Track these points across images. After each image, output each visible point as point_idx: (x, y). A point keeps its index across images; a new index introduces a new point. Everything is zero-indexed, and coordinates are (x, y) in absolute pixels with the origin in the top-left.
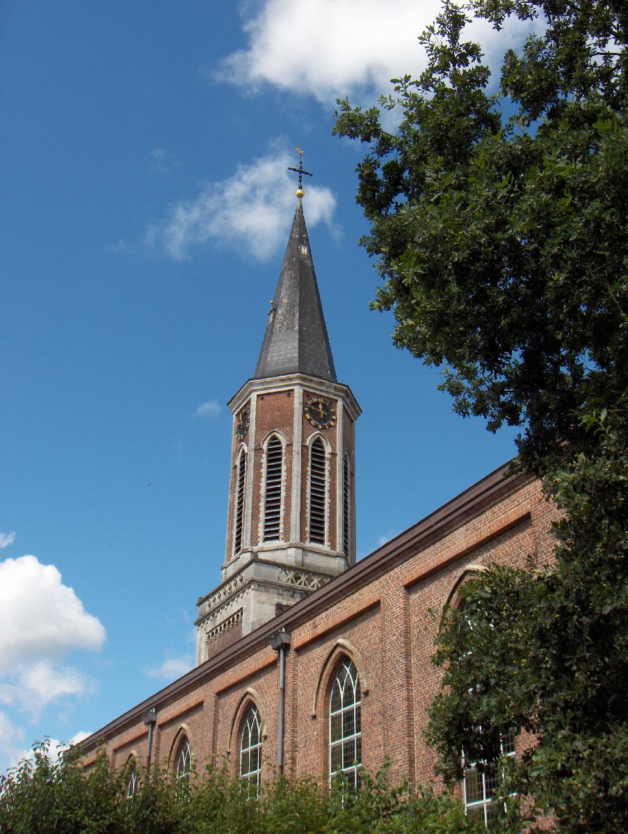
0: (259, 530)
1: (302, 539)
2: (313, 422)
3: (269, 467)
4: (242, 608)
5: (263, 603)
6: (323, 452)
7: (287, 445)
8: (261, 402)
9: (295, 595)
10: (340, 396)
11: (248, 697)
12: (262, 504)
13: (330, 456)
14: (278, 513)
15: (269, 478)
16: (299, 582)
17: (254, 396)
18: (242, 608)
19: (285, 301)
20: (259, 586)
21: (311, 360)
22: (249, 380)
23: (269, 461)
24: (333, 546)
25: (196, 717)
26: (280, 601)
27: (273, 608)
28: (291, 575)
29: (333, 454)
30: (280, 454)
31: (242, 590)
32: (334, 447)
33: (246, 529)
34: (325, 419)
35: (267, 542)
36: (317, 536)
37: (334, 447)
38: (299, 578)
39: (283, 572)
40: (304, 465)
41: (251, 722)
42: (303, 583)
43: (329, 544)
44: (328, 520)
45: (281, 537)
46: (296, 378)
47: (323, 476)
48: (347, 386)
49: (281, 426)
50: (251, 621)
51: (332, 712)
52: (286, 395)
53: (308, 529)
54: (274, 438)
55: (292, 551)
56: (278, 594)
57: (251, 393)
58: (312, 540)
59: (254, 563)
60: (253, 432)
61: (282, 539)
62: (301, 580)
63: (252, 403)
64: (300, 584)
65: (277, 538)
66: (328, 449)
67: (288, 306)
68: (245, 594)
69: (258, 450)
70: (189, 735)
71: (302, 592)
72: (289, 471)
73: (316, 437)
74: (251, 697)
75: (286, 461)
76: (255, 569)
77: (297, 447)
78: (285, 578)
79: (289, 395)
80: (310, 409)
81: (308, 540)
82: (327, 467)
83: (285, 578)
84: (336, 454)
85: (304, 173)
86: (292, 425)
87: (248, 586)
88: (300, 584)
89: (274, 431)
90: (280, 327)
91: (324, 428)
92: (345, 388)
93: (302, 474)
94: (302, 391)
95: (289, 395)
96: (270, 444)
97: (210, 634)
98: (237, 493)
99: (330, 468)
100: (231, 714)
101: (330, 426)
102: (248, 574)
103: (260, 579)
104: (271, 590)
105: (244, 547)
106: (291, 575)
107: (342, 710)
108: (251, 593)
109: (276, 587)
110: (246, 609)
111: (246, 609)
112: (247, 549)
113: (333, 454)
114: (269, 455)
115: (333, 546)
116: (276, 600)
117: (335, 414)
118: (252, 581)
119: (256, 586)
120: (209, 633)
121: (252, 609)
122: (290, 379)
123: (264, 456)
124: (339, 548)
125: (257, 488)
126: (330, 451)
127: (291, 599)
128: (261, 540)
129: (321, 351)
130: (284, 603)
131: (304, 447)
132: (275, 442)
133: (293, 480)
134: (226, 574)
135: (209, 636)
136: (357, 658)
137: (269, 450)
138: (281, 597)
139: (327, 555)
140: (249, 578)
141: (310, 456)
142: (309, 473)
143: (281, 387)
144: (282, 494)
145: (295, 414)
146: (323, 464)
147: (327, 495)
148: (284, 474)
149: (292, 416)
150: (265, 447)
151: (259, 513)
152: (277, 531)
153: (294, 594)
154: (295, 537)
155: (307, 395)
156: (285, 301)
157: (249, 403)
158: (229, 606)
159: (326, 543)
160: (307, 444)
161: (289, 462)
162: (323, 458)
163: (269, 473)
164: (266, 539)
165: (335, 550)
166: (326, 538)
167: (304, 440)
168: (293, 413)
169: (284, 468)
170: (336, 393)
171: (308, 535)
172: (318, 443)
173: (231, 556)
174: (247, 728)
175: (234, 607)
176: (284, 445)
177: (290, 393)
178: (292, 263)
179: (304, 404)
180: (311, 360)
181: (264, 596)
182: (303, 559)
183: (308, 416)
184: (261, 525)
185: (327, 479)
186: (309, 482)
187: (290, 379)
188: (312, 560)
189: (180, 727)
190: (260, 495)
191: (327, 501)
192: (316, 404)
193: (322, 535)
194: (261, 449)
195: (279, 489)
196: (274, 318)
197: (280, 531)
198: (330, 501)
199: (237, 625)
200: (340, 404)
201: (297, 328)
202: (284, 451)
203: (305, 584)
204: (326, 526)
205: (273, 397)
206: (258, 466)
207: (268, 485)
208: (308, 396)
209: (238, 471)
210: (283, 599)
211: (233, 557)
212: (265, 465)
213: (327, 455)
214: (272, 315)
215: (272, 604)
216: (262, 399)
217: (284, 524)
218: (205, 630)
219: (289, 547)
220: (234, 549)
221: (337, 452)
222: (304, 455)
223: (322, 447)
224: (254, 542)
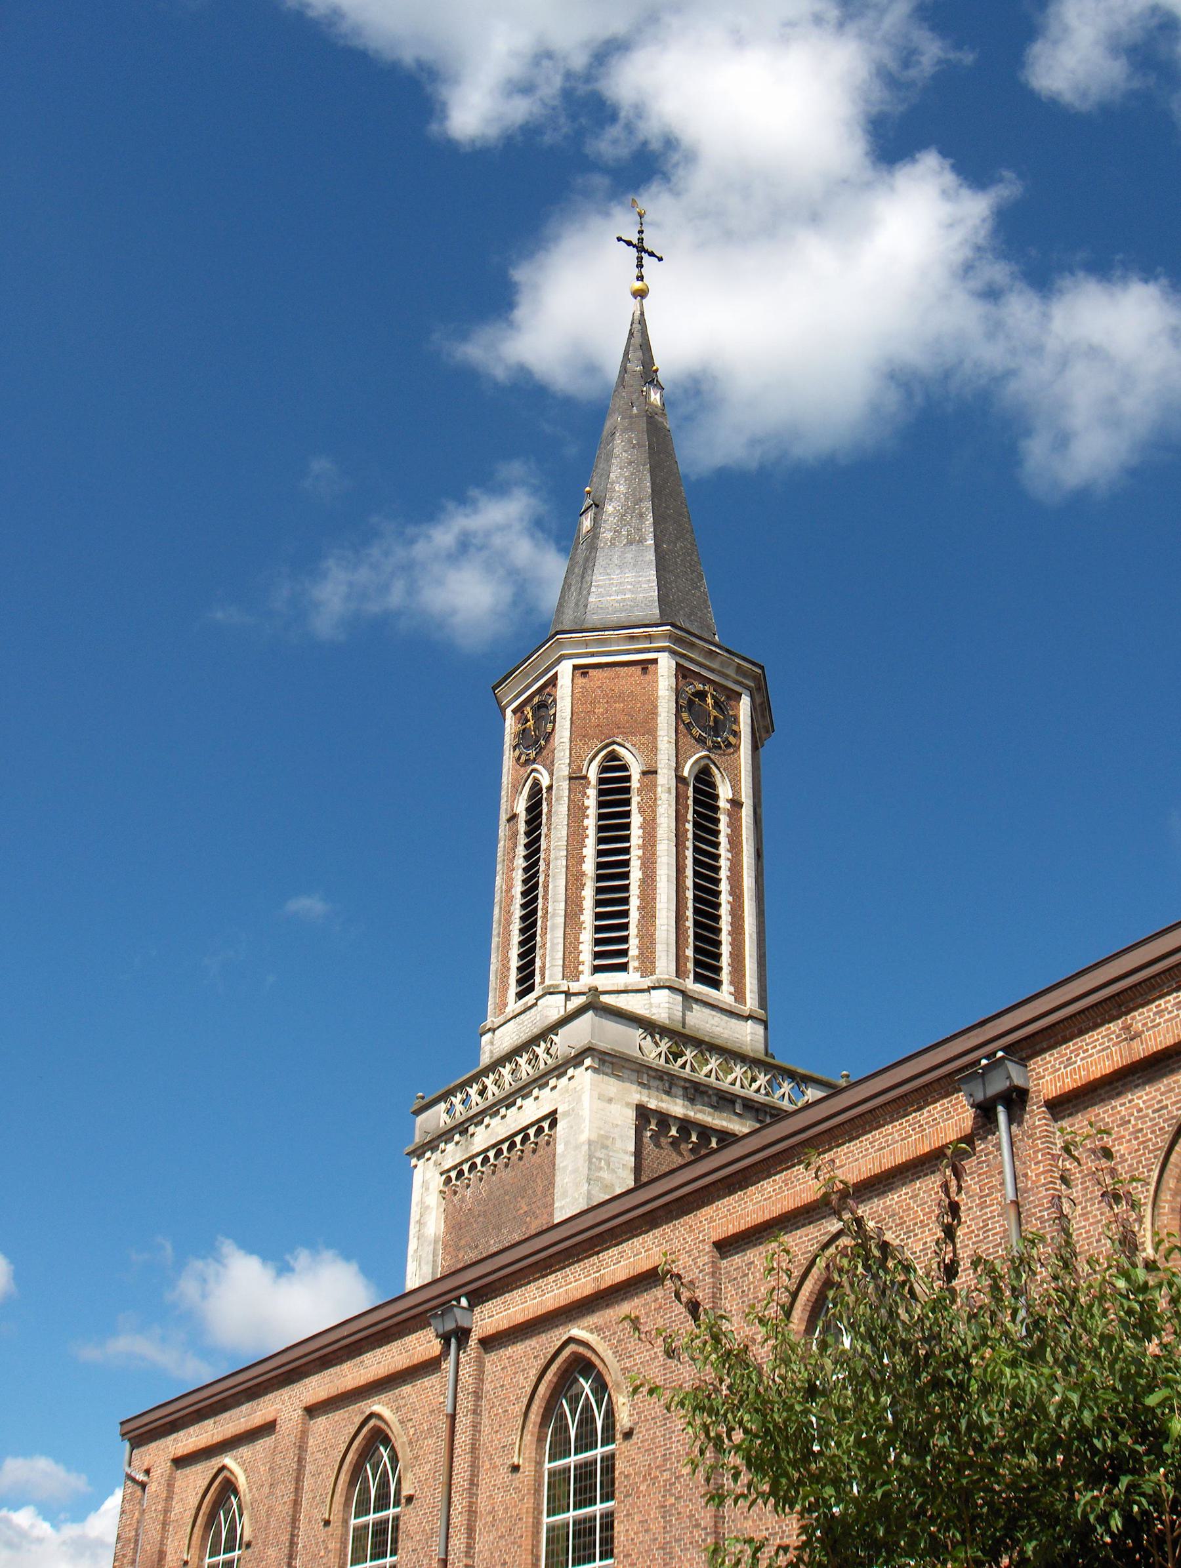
0: (581, 947)
1: (680, 972)
2: (696, 731)
3: (601, 817)
4: (555, 1112)
5: (610, 1100)
6: (716, 797)
7: (644, 773)
8: (581, 681)
9: (674, 1090)
10: (747, 687)
11: (225, 1473)
12: (588, 894)
13: (728, 806)
14: (625, 914)
15: (600, 841)
16: (680, 1061)
17: (565, 670)
18: (555, 1112)
19: (621, 488)
20: (602, 1062)
21: (682, 608)
22: (557, 633)
23: (601, 805)
24: (739, 995)
25: (263, 1445)
26: (645, 1099)
27: (631, 1114)
28: (665, 1045)
29: (736, 803)
30: (627, 790)
31: (559, 1070)
32: (736, 787)
33: (553, 945)
34: (717, 729)
35: (598, 975)
36: (708, 972)
37: (736, 787)
38: (681, 1055)
39: (649, 1038)
40: (679, 819)
41: (375, 1468)
42: (688, 1066)
43: (732, 989)
44: (729, 938)
45: (633, 964)
46: (663, 636)
47: (716, 845)
48: (762, 668)
49: (629, 732)
50: (584, 1137)
51: (550, 1462)
52: (637, 670)
53: (690, 952)
54: (613, 756)
55: (662, 997)
56: (640, 1084)
57: (558, 661)
58: (699, 978)
59: (590, 1014)
60: (567, 740)
61: (637, 970)
62: (684, 1059)
63: (560, 682)
64: (683, 1066)
65: (623, 967)
66: (724, 792)
67: (627, 499)
68: (564, 1080)
69: (577, 779)
70: (242, 1481)
71: (687, 1085)
72: (650, 826)
73: (703, 763)
74: (229, 1474)
75: (640, 808)
76: (593, 1025)
77: (665, 778)
78: (653, 1051)
79: (645, 670)
80: (690, 700)
81: (691, 976)
82: (723, 826)
83: (653, 1051)
84: (742, 805)
85: (646, 251)
86: (652, 732)
87: (576, 1060)
88: (683, 1066)
89: (614, 743)
90: (613, 539)
91: (717, 746)
92: (759, 671)
93: (677, 836)
94: (673, 663)
95: (645, 670)
96: (604, 769)
97: (453, 1174)
98: (520, 872)
99: (729, 831)
100: (194, 1501)
101: (729, 745)
102: (567, 1041)
103: (603, 1046)
104: (626, 1073)
105: (548, 982)
106: (665, 1045)
107: (572, 1460)
108: (583, 1077)
109: (634, 1067)
110: (567, 1114)
111: (567, 1114)
112: (557, 986)
113: (736, 803)
114: (601, 793)
115: (739, 995)
116: (637, 1095)
117: (736, 720)
118: (588, 1051)
119: (597, 1060)
120: (449, 1171)
121: (586, 1112)
122: (650, 638)
123: (592, 792)
124: (751, 1002)
125: (575, 857)
126: (730, 796)
127: (664, 1097)
128: (586, 968)
129: (698, 594)
130: (652, 1104)
131: (680, 779)
132: (614, 767)
133: (659, 847)
134: (492, 1043)
135: (449, 1179)
136: (399, 1437)
137: (601, 781)
138: (645, 1091)
139: (731, 1014)
140: (581, 1043)
141: (690, 802)
142: (690, 835)
143: (628, 652)
144: (632, 875)
145: (660, 709)
146: (716, 821)
147: (724, 887)
148: (636, 833)
149: (654, 713)
150: (593, 774)
151: (581, 911)
152: (624, 953)
153: (670, 1088)
154: (665, 966)
155: (682, 673)
156: (621, 488)
157: (553, 681)
158: (514, 1109)
159: (726, 987)
160: (686, 774)
161: (650, 808)
162: (716, 809)
163: (600, 829)
164: (597, 969)
165: (744, 1002)
166: (725, 976)
167: (678, 767)
168: (656, 707)
169: (636, 820)
170: (741, 679)
171: (690, 965)
172: (704, 780)
173: (506, 1005)
174: (366, 1479)
175: (530, 1110)
176: (635, 772)
177: (646, 666)
178: (631, 417)
179: (678, 692)
180: (682, 608)
181: (612, 1086)
182: (684, 1015)
183: (685, 715)
184: (587, 937)
185: (724, 850)
186: (689, 853)
187: (650, 638)
188: (702, 1021)
189: (220, 1465)
190: (583, 874)
191: (725, 898)
192: (702, 695)
193: (718, 970)
194: (585, 777)
195: (626, 863)
196: (596, 521)
197: (631, 953)
198: (731, 899)
199: (534, 1151)
200: (745, 703)
201: (651, 542)
202: (635, 784)
203: (693, 1070)
204: (725, 950)
205: (608, 672)
206: (576, 812)
207: (600, 853)
208: (684, 677)
209: (522, 827)
210: (649, 1096)
211: (513, 1006)
212: (592, 812)
213: (722, 804)
214: (590, 514)
215: (628, 1104)
216: (585, 674)
217: (641, 937)
218: (437, 1164)
219: (654, 988)
220: (513, 989)
221: (743, 800)
222: (679, 798)
223: (713, 785)
224: (571, 970)
